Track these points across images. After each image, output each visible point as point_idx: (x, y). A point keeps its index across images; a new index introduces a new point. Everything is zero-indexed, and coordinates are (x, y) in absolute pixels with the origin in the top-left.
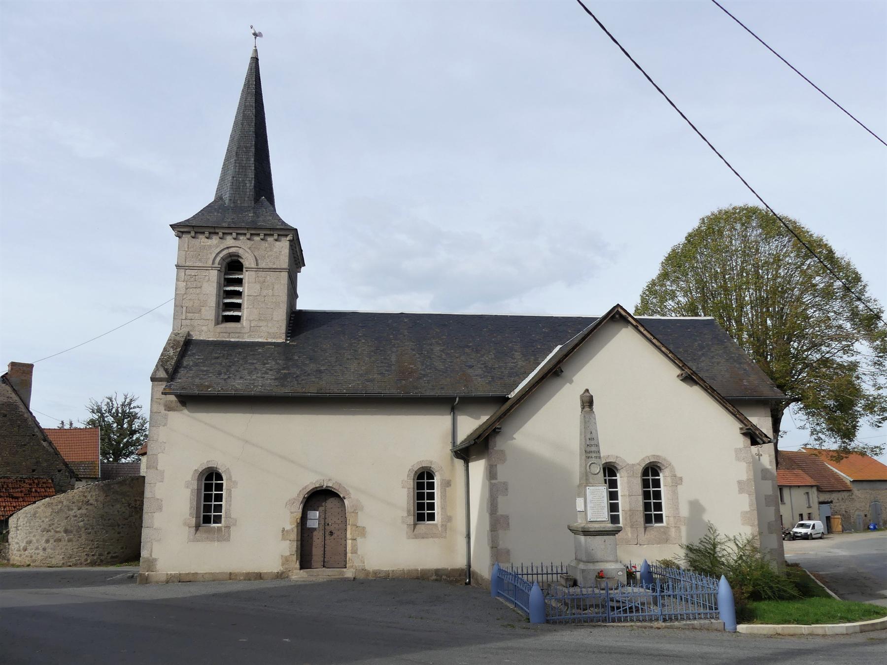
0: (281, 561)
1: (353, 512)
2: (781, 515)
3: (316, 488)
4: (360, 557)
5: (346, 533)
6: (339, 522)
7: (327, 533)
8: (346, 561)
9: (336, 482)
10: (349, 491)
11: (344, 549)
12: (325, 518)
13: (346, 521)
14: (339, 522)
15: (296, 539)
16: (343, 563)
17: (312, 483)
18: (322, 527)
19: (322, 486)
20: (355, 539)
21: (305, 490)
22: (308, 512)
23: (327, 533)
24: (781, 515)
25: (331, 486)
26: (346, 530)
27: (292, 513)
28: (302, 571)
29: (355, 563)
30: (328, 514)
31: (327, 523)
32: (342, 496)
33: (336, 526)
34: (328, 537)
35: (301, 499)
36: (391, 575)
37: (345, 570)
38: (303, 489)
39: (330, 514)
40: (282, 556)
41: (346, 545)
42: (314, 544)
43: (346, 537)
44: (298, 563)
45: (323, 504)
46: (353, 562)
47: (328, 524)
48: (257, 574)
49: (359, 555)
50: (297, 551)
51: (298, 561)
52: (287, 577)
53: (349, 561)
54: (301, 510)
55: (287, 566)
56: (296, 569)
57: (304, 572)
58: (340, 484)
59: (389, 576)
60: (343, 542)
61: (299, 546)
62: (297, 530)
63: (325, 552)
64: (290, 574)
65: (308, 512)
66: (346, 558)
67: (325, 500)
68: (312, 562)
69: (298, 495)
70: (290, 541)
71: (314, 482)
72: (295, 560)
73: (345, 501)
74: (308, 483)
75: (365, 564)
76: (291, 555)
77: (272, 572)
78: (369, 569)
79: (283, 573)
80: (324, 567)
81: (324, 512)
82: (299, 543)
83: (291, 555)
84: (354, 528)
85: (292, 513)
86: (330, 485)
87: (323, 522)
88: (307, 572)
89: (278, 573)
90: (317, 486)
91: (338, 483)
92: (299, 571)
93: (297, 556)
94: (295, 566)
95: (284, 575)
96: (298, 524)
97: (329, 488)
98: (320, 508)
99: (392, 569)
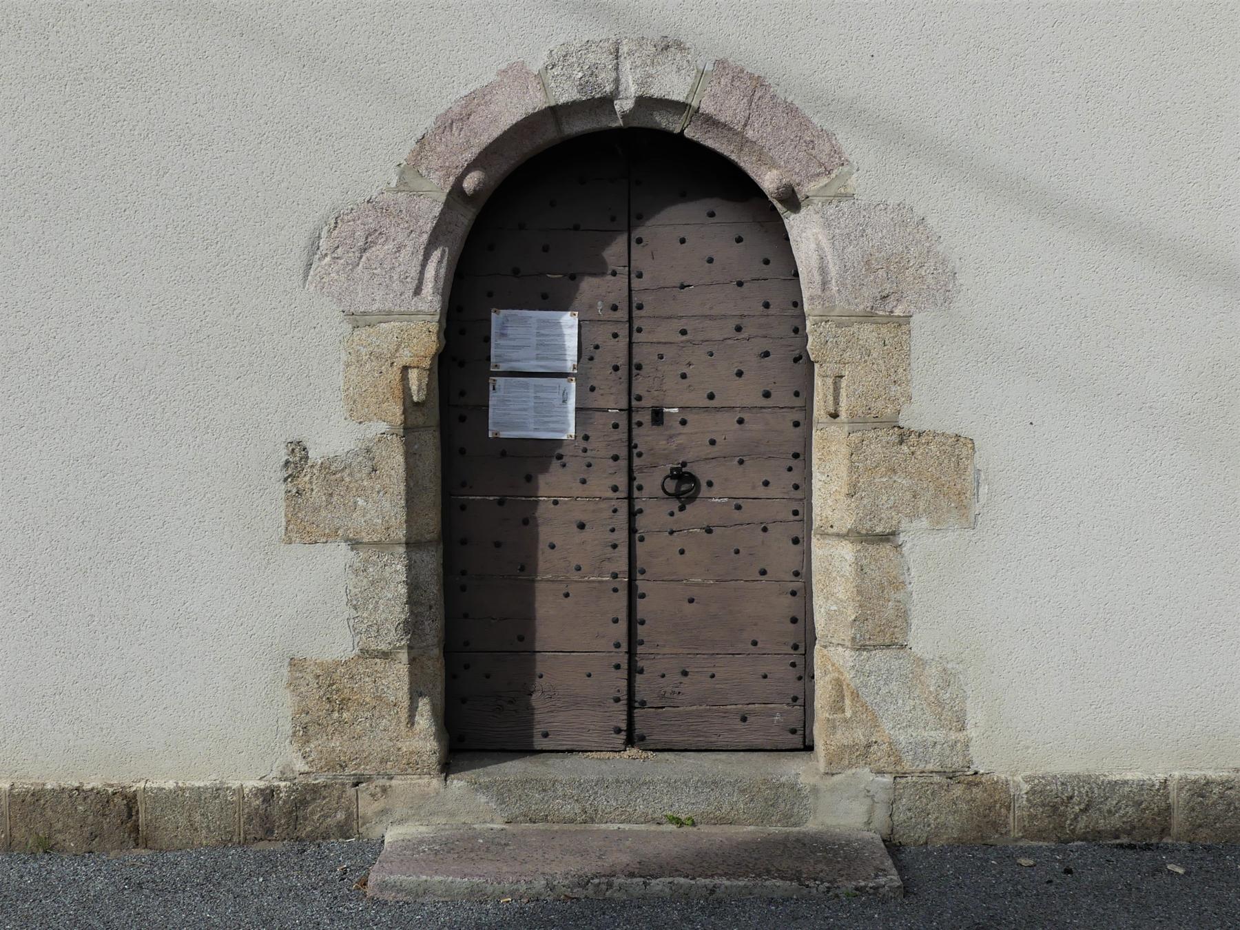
0: (286, 704)
1: (869, 316)
2: (850, 495)
3: (555, 113)
4: (932, 675)
5: (803, 488)
6: (746, 394)
7: (652, 481)
8: (804, 702)
9: (721, 64)
10: (830, 136)
11: (786, 605)
12: (634, 367)
13: (804, 392)
14: (746, 394)
15: (400, 534)
16: (783, 715)
17: (515, 73)
18: (606, 442)
19: (606, 102)
20: (887, 537)
21: (456, 137)
22: (497, 317)
23: (652, 481)
24: (850, 495)
25: (678, 95)
26: (802, 456)
27: (357, 319)
28: (458, 783)
29: (887, 725)
30: (656, 333)
31: (647, 402)
32: (769, 181)
33: (723, 427)
34: (655, 514)
35: (430, 206)
36: (1179, 820)
37: (796, 770)
38: (447, 124)
39: (667, 332)
40: (295, 664)
41: (802, 574)
42: (547, 564)
43: (802, 512)
44: (425, 721)
45: (614, 252)
46: (875, 724)
47: (658, 416)
48: (103, 800)
49: (921, 662)
50: (412, 627)
51: (424, 705)
52: (344, 830)
53: (837, 706)
54: (431, 300)
55: (335, 743)
56: (412, 766)
57: (478, 787)
58: (759, 83)
59: (1165, 831)
60: (782, 558)
61: (434, 590)
62: (409, 455)
63: (641, 631)
64: (367, 807)
65: (497, 317)
66: (807, 675)
67: (631, 220)
68: (536, 700)
69: (411, 169)
70: (355, 544)
71: (536, 67)
72: (403, 696)
73: (794, 223)
74: (491, 77)
75: (972, 732)
76: (366, 654)
77: (217, 791)
78: (1001, 774)
79: (305, 797)
80: (630, 741)
81: (622, 314)
82: (431, 561)
83: (366, 654)
84: (878, 445)
85: (357, 319)
86: (673, 86)
87: (612, 399)
88: (502, 794)
89: (269, 794)
90: (566, 94)
91: (737, 75)
92: (436, 783)
93: (412, 661)
94: (405, 746)
95: (314, 812)
96: (410, 407)
97: (666, 122)
98: (588, 285)
99: (1194, 774)
